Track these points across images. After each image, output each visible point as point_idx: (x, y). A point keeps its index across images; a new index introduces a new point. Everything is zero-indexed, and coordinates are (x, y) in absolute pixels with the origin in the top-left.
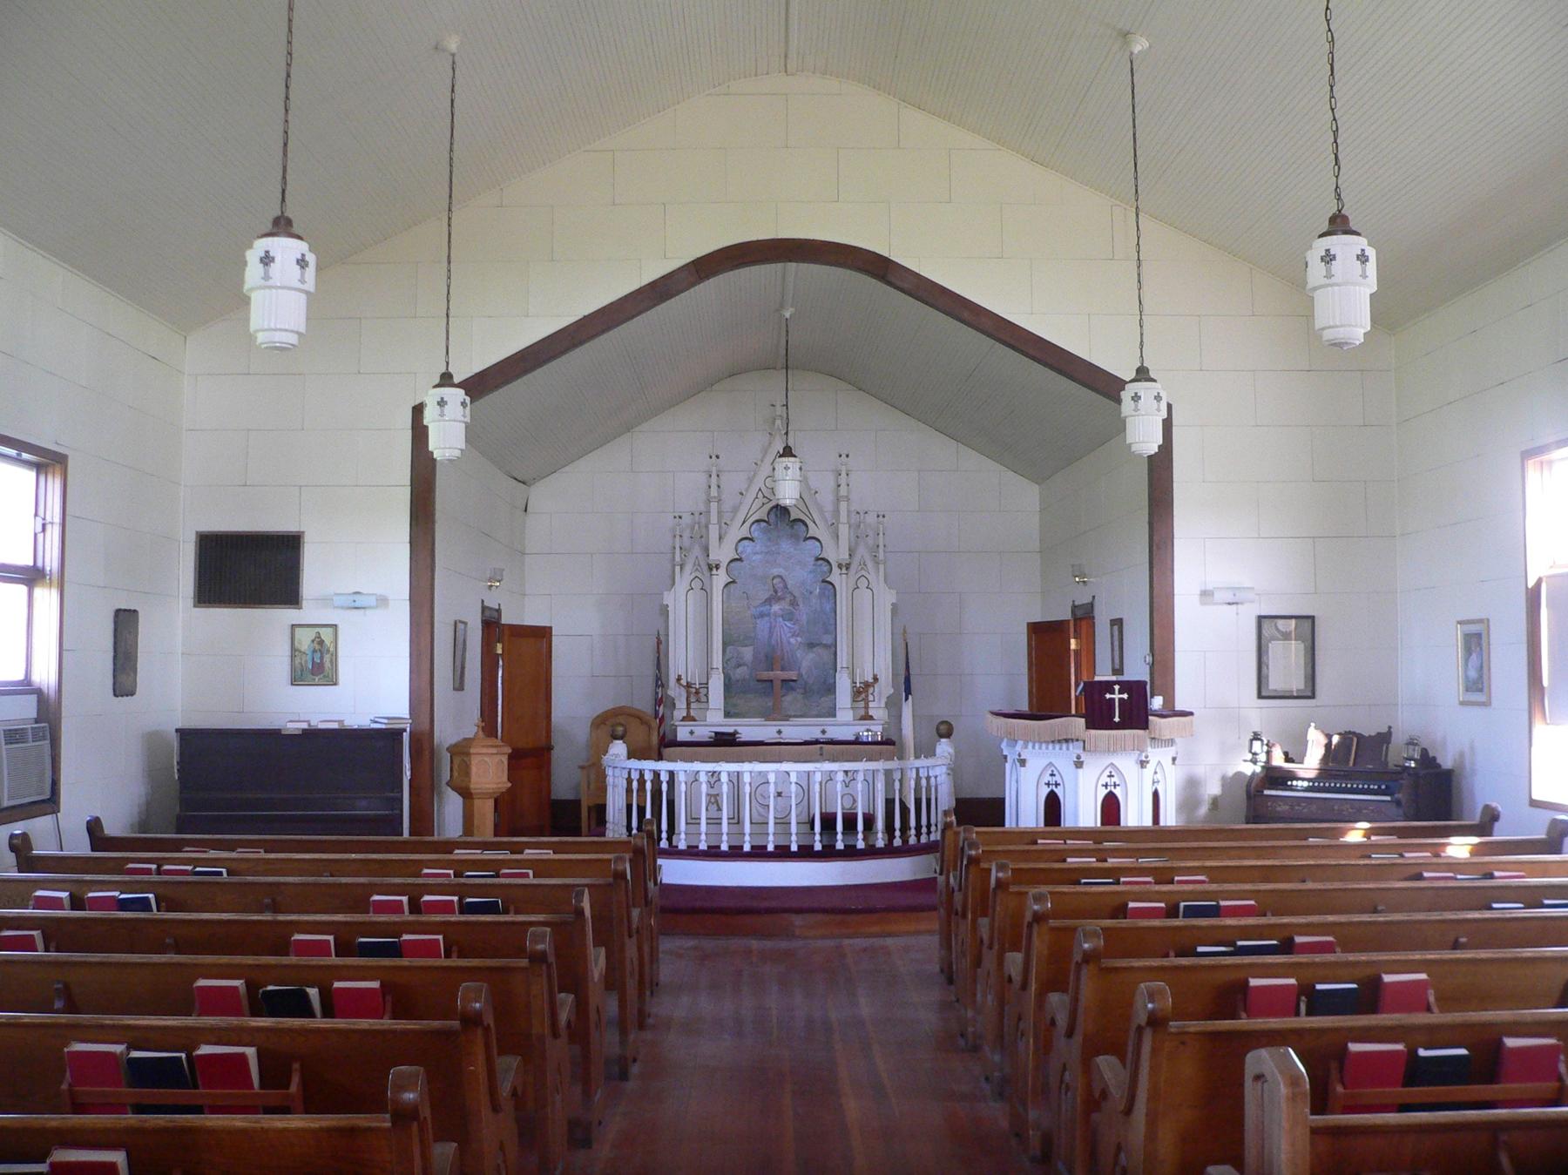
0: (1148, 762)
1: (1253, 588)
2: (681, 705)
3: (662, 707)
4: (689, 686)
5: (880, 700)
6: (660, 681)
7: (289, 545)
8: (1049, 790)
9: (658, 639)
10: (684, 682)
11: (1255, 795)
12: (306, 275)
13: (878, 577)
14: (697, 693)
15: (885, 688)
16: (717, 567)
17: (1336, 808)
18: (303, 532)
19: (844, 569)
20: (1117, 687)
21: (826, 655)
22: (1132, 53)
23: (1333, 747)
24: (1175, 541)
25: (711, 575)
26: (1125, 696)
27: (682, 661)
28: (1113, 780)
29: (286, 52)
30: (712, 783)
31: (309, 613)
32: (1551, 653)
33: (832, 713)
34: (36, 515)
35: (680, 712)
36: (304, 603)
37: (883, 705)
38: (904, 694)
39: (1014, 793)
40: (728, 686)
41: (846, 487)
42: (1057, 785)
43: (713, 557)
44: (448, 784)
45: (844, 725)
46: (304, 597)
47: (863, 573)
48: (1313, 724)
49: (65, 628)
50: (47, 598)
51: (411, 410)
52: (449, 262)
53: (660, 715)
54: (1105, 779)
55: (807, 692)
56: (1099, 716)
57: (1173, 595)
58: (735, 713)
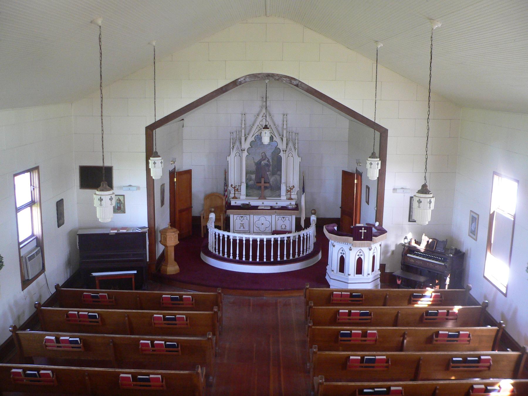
0: (372, 249)
2: (232, 192)
3: (226, 192)
4: (234, 188)
5: (295, 192)
6: (226, 185)
7: (109, 171)
8: (341, 255)
9: (225, 171)
10: (233, 186)
11: (404, 255)
12: (113, 203)
14: (237, 189)
15: (297, 188)
16: (244, 150)
17: (428, 264)
18: (113, 166)
20: (363, 228)
22: (377, 48)
23: (429, 243)
25: (242, 153)
26: (366, 231)
27: (233, 179)
28: (361, 254)
29: (100, 97)
31: (116, 191)
32: (494, 235)
34: (31, 185)
35: (232, 195)
36: (114, 188)
37: (296, 194)
39: (331, 253)
40: (247, 187)
41: (286, 125)
42: (344, 254)
44: (160, 241)
45: (283, 202)
47: (291, 152)
48: (424, 234)
49: (43, 219)
50: (36, 210)
51: (145, 128)
52: (155, 116)
53: (226, 195)
54: (358, 253)
56: (357, 237)
57: (384, 189)
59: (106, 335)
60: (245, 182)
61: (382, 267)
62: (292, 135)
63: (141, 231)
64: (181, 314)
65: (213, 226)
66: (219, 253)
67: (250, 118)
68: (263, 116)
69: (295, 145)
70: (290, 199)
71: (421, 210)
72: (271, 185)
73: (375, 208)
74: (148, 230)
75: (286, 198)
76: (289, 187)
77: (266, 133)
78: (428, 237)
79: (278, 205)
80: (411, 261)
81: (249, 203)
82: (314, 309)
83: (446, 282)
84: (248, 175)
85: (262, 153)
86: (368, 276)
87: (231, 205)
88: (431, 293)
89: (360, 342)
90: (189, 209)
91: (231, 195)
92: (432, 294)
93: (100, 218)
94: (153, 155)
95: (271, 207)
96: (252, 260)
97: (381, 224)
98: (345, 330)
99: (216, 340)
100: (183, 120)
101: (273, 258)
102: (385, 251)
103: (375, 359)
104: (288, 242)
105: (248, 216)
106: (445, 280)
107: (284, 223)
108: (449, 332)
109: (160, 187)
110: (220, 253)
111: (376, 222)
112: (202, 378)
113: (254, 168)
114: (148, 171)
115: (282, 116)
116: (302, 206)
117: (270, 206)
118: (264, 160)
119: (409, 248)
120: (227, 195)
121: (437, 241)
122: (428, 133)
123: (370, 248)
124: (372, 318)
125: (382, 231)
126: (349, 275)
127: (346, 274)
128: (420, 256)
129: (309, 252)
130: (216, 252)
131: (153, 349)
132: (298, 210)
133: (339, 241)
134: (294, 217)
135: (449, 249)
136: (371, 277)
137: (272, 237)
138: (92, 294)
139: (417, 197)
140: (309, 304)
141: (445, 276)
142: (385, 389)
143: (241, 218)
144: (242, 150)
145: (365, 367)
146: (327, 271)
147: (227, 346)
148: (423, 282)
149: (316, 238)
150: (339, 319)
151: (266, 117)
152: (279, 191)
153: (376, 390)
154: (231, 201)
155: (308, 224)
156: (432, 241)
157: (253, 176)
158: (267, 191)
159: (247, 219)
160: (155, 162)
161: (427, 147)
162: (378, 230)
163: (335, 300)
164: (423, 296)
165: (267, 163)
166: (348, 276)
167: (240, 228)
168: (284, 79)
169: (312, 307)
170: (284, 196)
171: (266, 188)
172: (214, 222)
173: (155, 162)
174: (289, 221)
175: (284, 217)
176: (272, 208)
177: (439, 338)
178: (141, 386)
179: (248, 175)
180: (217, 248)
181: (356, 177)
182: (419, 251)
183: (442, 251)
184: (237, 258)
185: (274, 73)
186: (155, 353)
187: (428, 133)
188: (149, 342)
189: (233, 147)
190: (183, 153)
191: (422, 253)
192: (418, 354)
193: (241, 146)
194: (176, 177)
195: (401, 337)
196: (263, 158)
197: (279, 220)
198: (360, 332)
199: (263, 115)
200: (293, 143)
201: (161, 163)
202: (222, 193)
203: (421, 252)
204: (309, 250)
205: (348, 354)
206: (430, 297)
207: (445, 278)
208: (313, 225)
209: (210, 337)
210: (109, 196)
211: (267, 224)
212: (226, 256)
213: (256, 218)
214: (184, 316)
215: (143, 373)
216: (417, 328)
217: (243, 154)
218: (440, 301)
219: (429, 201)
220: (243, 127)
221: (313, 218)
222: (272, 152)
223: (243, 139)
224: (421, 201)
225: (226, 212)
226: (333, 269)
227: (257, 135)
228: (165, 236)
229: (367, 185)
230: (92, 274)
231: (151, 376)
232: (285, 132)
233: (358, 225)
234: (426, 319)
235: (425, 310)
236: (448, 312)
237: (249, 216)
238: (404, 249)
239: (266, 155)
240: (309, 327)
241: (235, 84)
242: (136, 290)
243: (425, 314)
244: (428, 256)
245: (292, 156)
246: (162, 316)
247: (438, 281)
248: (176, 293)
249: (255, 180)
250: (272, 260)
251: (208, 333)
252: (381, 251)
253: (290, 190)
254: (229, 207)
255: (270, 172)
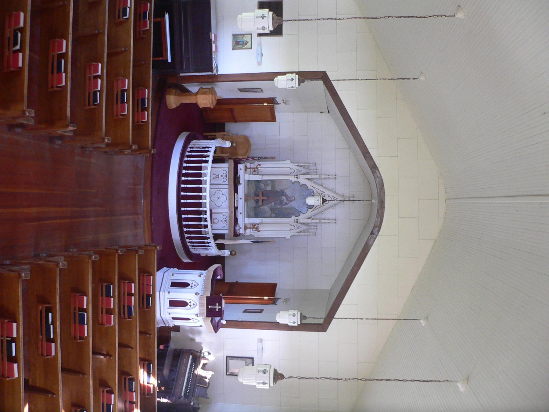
0: (197, 317)
1: (262, 356)
4: (257, 168)
5: (253, 233)
6: (260, 159)
9: (275, 158)
10: (258, 167)
13: (295, 233)
14: (255, 171)
15: (257, 235)
16: (297, 178)
19: (296, 221)
20: (220, 307)
21: (269, 214)
22: (420, 320)
23: (204, 379)
24: (279, 331)
25: (295, 176)
26: (217, 310)
27: (266, 166)
28: (192, 305)
30: (223, 176)
33: (249, 216)
35: (249, 165)
38: (253, 241)
40: (258, 181)
42: (192, 287)
43: (301, 176)
44: (202, 88)
45: (242, 220)
46: (261, 38)
47: (296, 227)
48: (214, 373)
51: (325, 71)
53: (249, 159)
54: (192, 302)
55: (256, 208)
56: (210, 301)
58: (249, 184)
59: (107, 25)
60: (263, 179)
61: (177, 329)
62: (315, 229)
63: (213, 67)
64: (128, 109)
65: (217, 145)
66: (189, 152)
67: (330, 184)
68: (334, 198)
69: (303, 232)
70: (246, 228)
71: (255, 373)
72: (261, 208)
73: (240, 320)
74: (215, 75)
75: (246, 224)
76: (258, 227)
77: (318, 201)
78: (210, 378)
79: (239, 215)
80: (185, 360)
81: (241, 184)
82: (135, 255)
83: (163, 398)
84: (271, 182)
85: (294, 197)
86: (168, 314)
87: (239, 165)
88: (153, 383)
89: (100, 307)
90: (234, 120)
91: (249, 164)
92: (152, 384)
93: (242, 17)
94: (301, 79)
95: (237, 208)
96: (182, 188)
97: (224, 326)
98: (114, 290)
99: (102, 148)
100: (329, 112)
101: (184, 210)
102: (194, 331)
103: (84, 324)
104: (200, 226)
105: (227, 182)
106: (165, 397)
107: (220, 221)
108: (113, 405)
109: (259, 88)
110: (189, 153)
111: (226, 320)
112: (62, 132)
113: (278, 188)
114: (284, 73)
115: (333, 217)
116: (239, 240)
117: (238, 207)
118: (287, 200)
119: (198, 357)
120: (249, 160)
121: (207, 388)
122: (341, 379)
123: (198, 315)
124: (125, 319)
125: (216, 327)
126: (169, 293)
127: (169, 290)
128: (190, 369)
129: (191, 248)
130: (190, 148)
131: (92, 78)
132: (234, 237)
133: (205, 281)
134: (226, 232)
135: (198, 401)
136: (166, 317)
137: (207, 209)
138: (149, 13)
139: (270, 369)
140: (140, 250)
141: (169, 398)
142: (52, 337)
143: (225, 175)
144: (297, 175)
145: (75, 313)
146: (172, 269)
147: (93, 160)
148: (162, 373)
149: (205, 256)
150: (123, 282)
151: (333, 201)
152: (254, 216)
153: (52, 326)
154: (243, 164)
155: (221, 247)
156: (207, 382)
157: (269, 188)
158: (254, 202)
159: (223, 181)
160: (293, 81)
161: (325, 378)
162: (218, 323)
163: (143, 278)
164: (149, 374)
165: (284, 203)
166: (168, 292)
167: (214, 174)
168: (379, 220)
169: (137, 253)
170: (248, 221)
171: (257, 202)
172: (221, 146)
173: (294, 80)
174: (223, 228)
175: (226, 222)
176: (236, 208)
177: (106, 394)
178: (53, 64)
179: (270, 182)
180: (194, 149)
181: (271, 298)
182: (196, 368)
183: (196, 394)
184: (184, 171)
185: (385, 208)
186: (87, 81)
187: (341, 379)
188: (99, 73)
189: (301, 166)
190: (292, 113)
191: (193, 372)
192: (91, 372)
193: (302, 175)
194: (268, 105)
195: (107, 352)
196: (289, 198)
197: (223, 216)
198: (112, 307)
199: (335, 198)
200: (305, 230)
201: (293, 87)
202: (250, 155)
203: (194, 370)
204: (193, 249)
205: (89, 295)
206: (148, 382)
207: (167, 397)
208: (220, 252)
209: (106, 140)
210: (267, 26)
211: (219, 203)
212: (186, 159)
213: (225, 191)
214: (126, 113)
215: (66, 65)
216: (117, 369)
217: (294, 177)
218: (144, 393)
219: (266, 382)
220: (322, 176)
221: (226, 253)
222: (296, 207)
223: (309, 177)
224: (265, 374)
225: (231, 159)
226: (174, 275)
227: (313, 192)
228: (208, 93)
229: (264, 310)
230: (168, 14)
231: (64, 75)
232: (318, 221)
233: (223, 301)
234: (125, 379)
235: (135, 378)
236: (134, 403)
237: (227, 184)
238: (197, 352)
239: (292, 201)
240: (117, 250)
241: (374, 167)
242: (153, 61)
243: (131, 377)
244: (190, 378)
245: (291, 229)
246: (126, 88)
247: (163, 389)
248: (149, 103)
249: (266, 190)
250: (183, 209)
251: (110, 138)
252: (186, 327)
253: (256, 227)
254: (237, 163)
255: (274, 205)
